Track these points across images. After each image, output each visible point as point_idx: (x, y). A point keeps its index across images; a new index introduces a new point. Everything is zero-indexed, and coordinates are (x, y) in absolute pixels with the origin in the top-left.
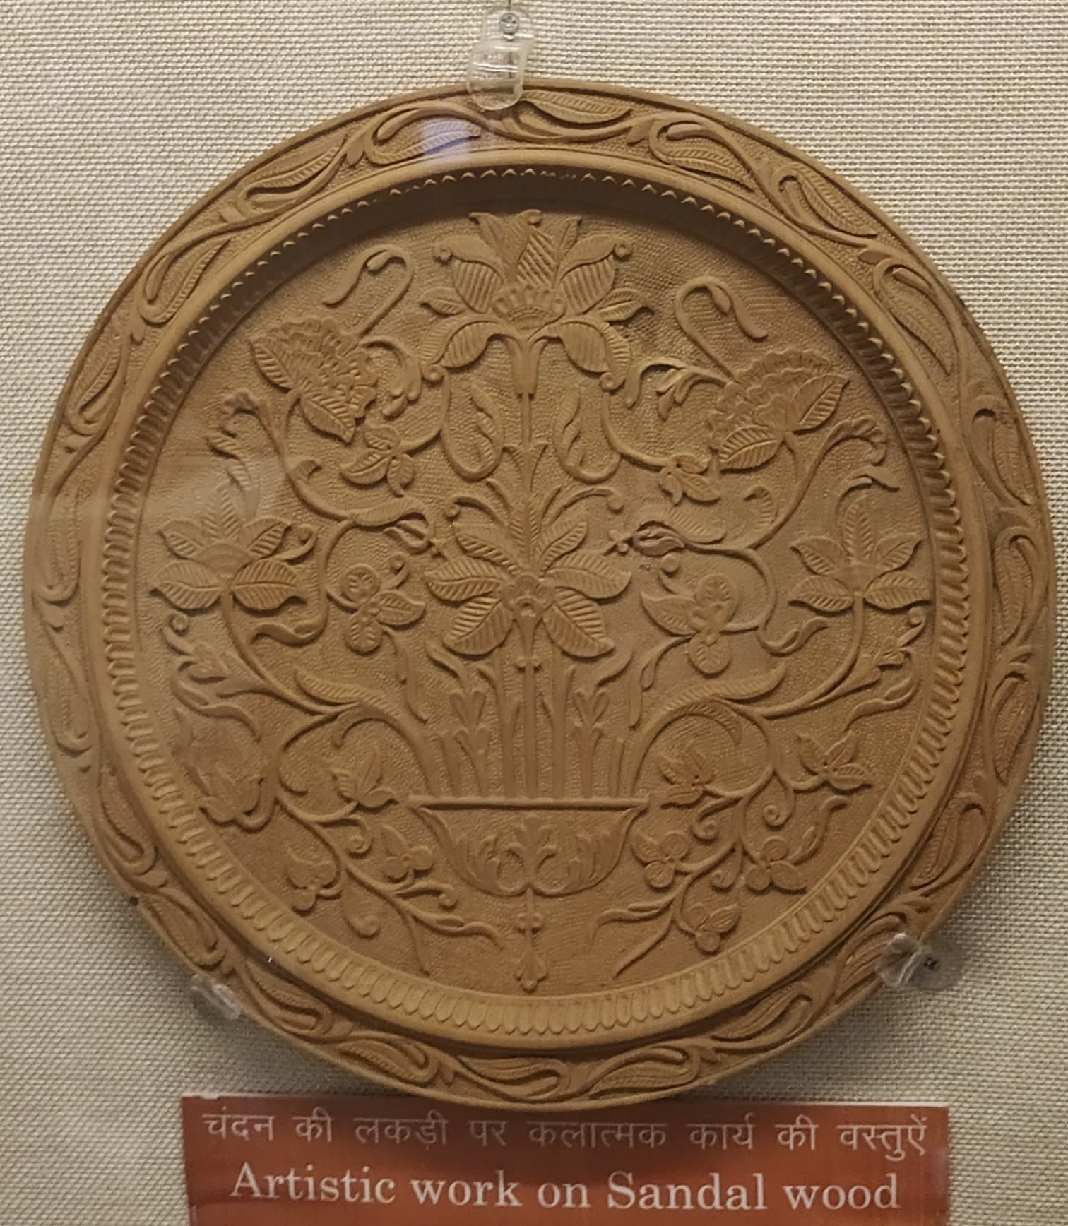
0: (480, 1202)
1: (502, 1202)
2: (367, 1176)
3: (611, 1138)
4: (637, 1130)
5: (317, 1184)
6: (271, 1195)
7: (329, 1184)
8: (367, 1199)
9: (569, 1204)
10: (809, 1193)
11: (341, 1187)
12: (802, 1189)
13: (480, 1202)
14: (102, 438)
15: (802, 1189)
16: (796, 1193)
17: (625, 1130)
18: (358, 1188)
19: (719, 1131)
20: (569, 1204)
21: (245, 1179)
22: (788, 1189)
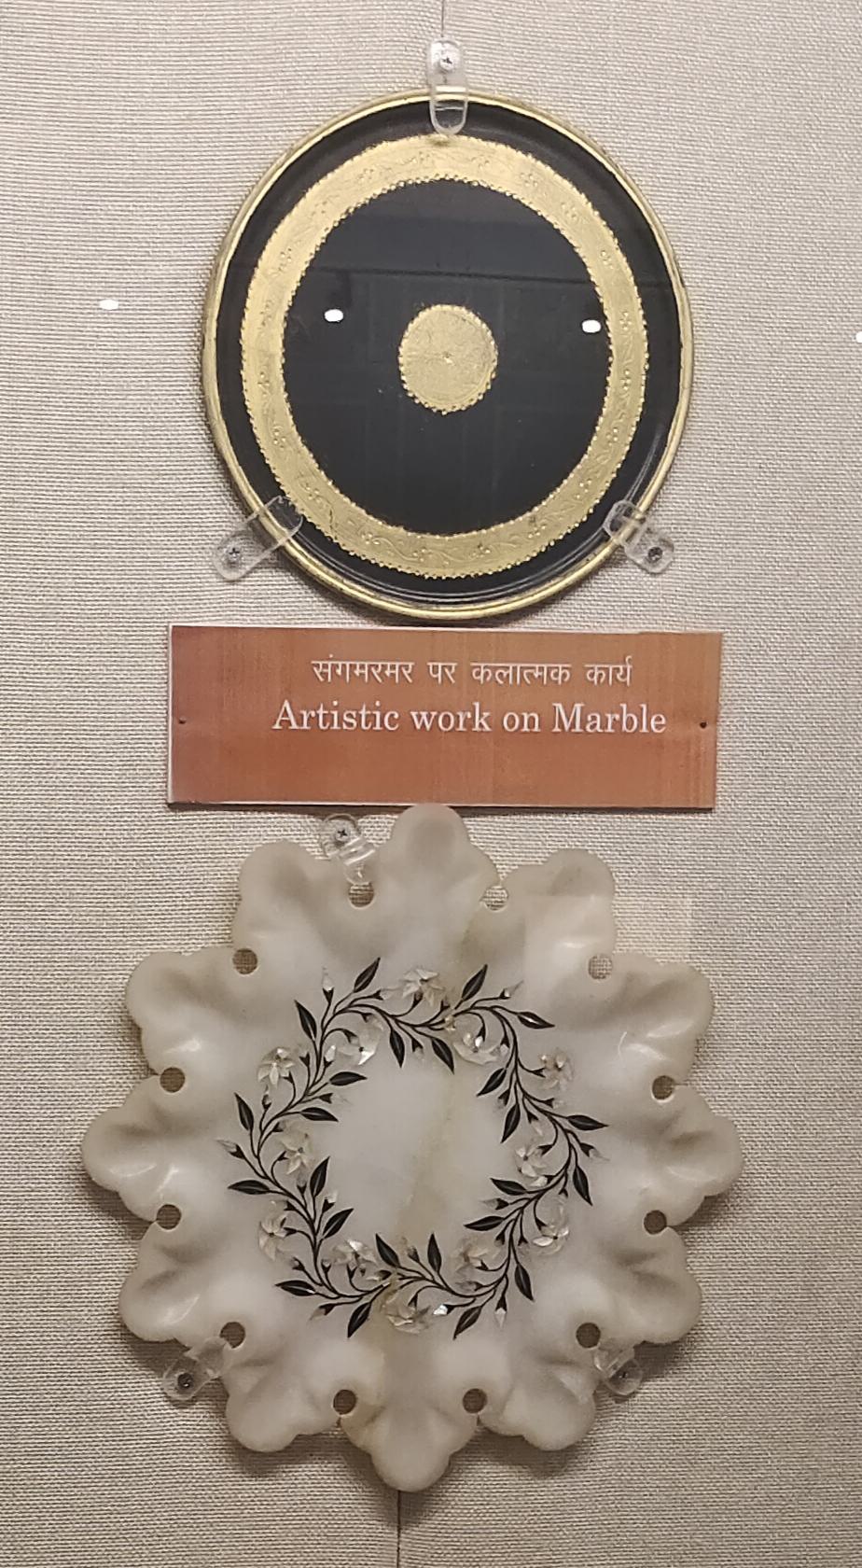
0: (461, 728)
1: (477, 728)
2: (336, 708)
3: (530, 675)
4: (549, 670)
5: (340, 718)
6: (610, 729)
7: (350, 716)
8: (378, 727)
9: (526, 729)
10: (429, 717)
11: (359, 718)
12: (424, 714)
13: (461, 728)
14: (139, 1030)
15: (424, 714)
16: (419, 717)
17: (393, 667)
18: (370, 718)
19: (607, 670)
20: (526, 729)
21: (286, 714)
22: (414, 714)
